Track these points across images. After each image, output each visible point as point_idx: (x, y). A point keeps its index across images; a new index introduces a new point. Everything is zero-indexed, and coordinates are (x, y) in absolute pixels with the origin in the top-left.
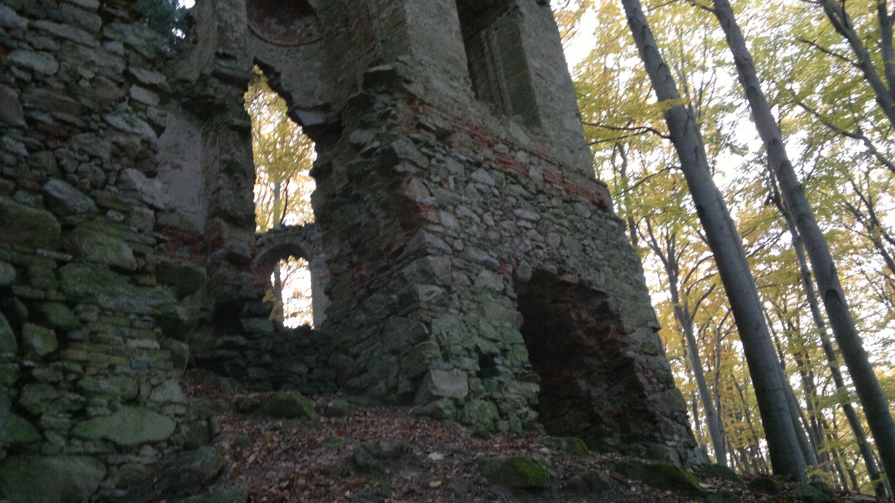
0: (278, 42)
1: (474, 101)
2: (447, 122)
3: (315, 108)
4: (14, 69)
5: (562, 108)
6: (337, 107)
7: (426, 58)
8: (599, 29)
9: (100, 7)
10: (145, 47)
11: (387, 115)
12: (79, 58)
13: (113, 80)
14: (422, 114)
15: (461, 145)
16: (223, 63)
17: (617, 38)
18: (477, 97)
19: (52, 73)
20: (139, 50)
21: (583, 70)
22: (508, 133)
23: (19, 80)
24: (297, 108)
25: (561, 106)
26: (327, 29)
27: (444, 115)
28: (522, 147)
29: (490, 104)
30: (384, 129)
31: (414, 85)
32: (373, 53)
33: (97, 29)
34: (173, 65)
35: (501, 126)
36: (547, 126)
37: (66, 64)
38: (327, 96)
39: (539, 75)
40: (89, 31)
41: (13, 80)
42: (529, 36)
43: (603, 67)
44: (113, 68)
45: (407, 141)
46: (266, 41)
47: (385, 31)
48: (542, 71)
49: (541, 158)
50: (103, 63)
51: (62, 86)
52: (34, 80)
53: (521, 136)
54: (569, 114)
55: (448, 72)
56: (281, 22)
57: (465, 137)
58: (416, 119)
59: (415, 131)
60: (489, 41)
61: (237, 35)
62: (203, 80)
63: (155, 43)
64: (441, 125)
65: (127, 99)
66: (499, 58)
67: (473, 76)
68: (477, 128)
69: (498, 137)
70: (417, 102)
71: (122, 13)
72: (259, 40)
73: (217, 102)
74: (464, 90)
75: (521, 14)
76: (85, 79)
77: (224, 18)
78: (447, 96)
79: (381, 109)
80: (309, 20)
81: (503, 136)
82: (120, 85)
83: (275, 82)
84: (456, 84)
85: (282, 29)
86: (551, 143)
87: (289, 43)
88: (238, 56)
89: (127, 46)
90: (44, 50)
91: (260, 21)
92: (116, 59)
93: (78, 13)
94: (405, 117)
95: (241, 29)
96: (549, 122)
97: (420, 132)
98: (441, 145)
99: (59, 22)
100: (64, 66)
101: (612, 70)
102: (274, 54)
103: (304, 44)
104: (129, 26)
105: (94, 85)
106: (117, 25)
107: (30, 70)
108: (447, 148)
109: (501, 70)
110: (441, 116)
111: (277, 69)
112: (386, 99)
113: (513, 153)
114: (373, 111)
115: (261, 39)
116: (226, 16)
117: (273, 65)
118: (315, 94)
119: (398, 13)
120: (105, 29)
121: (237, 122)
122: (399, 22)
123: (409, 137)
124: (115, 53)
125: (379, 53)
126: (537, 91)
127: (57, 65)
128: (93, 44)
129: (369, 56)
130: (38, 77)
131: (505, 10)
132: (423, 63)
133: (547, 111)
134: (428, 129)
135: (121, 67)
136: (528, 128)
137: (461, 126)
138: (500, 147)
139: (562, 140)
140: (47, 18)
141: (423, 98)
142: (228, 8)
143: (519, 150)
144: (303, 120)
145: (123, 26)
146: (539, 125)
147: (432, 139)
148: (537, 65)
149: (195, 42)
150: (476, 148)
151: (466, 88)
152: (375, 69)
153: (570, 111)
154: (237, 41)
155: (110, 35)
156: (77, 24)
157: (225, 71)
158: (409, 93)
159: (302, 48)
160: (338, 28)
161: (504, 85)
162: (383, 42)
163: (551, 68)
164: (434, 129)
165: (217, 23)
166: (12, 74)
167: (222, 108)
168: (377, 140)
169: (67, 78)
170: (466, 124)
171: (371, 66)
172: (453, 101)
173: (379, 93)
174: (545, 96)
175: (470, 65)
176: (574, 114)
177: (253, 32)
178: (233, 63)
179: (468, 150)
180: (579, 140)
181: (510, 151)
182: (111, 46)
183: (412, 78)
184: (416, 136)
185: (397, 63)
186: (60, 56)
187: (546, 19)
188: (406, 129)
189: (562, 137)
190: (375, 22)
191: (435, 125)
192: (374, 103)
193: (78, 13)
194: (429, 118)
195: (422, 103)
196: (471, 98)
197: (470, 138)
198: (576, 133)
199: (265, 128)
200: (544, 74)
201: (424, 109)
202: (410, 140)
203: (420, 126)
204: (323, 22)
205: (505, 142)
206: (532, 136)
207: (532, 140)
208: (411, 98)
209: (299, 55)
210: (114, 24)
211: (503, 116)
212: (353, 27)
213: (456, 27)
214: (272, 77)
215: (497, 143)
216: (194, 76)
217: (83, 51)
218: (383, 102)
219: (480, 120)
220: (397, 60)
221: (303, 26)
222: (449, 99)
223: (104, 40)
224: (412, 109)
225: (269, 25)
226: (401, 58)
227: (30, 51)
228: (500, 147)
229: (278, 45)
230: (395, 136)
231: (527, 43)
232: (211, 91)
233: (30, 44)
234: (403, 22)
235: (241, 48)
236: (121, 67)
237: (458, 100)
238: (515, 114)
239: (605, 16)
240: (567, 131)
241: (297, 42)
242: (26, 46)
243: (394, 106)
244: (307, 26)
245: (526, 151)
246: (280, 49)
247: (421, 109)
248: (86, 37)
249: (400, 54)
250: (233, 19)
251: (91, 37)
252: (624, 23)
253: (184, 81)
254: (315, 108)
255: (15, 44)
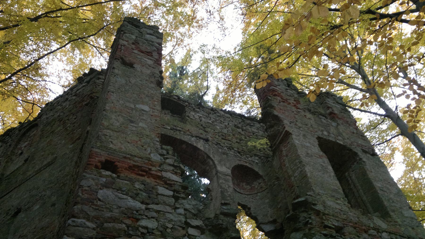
0: (247, 193)
1: (351, 209)
2: (339, 222)
3: (270, 222)
4: (140, 228)
5: (400, 205)
6: (279, 221)
7: (321, 191)
8: (405, 160)
9: (174, 194)
10: (193, 208)
11: (307, 223)
12: (166, 219)
13: (181, 227)
14: (325, 220)
15: (350, 233)
16: (224, 207)
17: (417, 163)
18: (351, 207)
19: (155, 228)
20: (190, 210)
21: (403, 181)
22: (374, 223)
23: (142, 233)
24: (261, 223)
25: (399, 204)
26: (269, 184)
27: (337, 219)
28: (384, 230)
29: (360, 209)
30: (307, 231)
31: (318, 205)
32: (294, 193)
33: (173, 204)
34: (203, 211)
35: (370, 220)
36: (394, 216)
37: (161, 222)
38: (274, 216)
39: (383, 191)
40: (170, 206)
41: (140, 234)
42: (371, 172)
43: (413, 178)
44: (180, 221)
45: (321, 236)
46: (242, 194)
47: (298, 182)
48: (383, 188)
49: (397, 235)
50: (176, 219)
51: (159, 233)
52: (148, 232)
53: (383, 225)
54: (405, 208)
55: (334, 196)
56: (248, 184)
57: (351, 229)
58: (323, 223)
59: (324, 229)
60: (350, 177)
61: (229, 193)
62: (216, 216)
63: (197, 206)
64: (336, 224)
65: (187, 234)
66: (358, 185)
67: (346, 196)
68: (356, 223)
69: (369, 227)
70: (321, 214)
71: (182, 195)
72: (239, 194)
73: (224, 226)
74: (344, 204)
75: (364, 162)
76: (169, 228)
77: (223, 187)
78: (336, 208)
79: (304, 220)
80: (260, 181)
81: (372, 225)
82: (183, 228)
83: (249, 212)
84: (339, 202)
85: (249, 187)
86: (400, 225)
87: (253, 193)
88: (231, 203)
89: (185, 210)
90: (152, 218)
91: (238, 185)
92: (181, 216)
93: (165, 199)
94: (317, 223)
95: (231, 190)
96: (395, 214)
97: (326, 230)
98: (339, 235)
99: (157, 204)
100: (160, 224)
101: (419, 179)
102: (246, 199)
103: (260, 192)
104: (186, 200)
105: (173, 230)
106: (181, 201)
107: (146, 228)
108: (343, 237)
109: (361, 190)
110: (335, 220)
111: (249, 206)
112: (305, 215)
113: (379, 234)
114: (300, 222)
115: (240, 193)
116: (223, 186)
117: (247, 204)
118: (268, 215)
119: (302, 173)
120: (176, 204)
121: (234, 235)
122: (304, 176)
123: (320, 233)
124: (180, 214)
125: (297, 192)
126: (383, 199)
127: (157, 223)
128: (171, 212)
129: (293, 195)
130: (150, 231)
131: (355, 162)
132: (320, 194)
133: (392, 208)
134: (330, 228)
135: (183, 220)
136: (384, 219)
137: (348, 224)
138: (372, 232)
139: (405, 223)
140: (153, 203)
141: (324, 211)
142: (224, 182)
143: (382, 232)
144: (264, 229)
145: (183, 201)
146: (390, 216)
147: (334, 233)
148: (379, 185)
149: (211, 200)
150: (358, 234)
151: (345, 203)
152: (297, 201)
153: (405, 206)
154: (230, 196)
155: (178, 206)
156: (165, 203)
157: (226, 211)
158: (316, 210)
159: (259, 194)
160: (274, 182)
161: (365, 198)
162: (298, 187)
163: (388, 186)
164: (333, 227)
165: (220, 190)
166: (139, 231)
167: (226, 229)
168: (305, 237)
169: (161, 229)
170: (350, 222)
171: (294, 199)
172: (340, 211)
173: (301, 212)
174: (389, 200)
175: (344, 190)
176: (408, 207)
177: (236, 190)
178: (229, 207)
179: (354, 236)
180: (415, 221)
181: (378, 234)
182: (179, 211)
183: (316, 202)
184: (325, 232)
185: (307, 196)
186: (158, 219)
187: (377, 162)
188: (319, 229)
189: (405, 221)
190: (293, 178)
191: (334, 225)
192: (299, 218)
193: (165, 199)
194: (329, 222)
195: (324, 214)
196: (349, 208)
197: (353, 229)
198: (412, 218)
199: (245, 234)
200: (385, 189)
201: (326, 217)
202: (322, 235)
203: (326, 227)
204: (266, 181)
205: (374, 229)
206: (387, 223)
207: (388, 225)
208: (318, 213)
209: (258, 198)
210: (179, 201)
211: (369, 215)
212: (282, 181)
213: (333, 174)
214: (247, 210)
215: (369, 230)
216: (212, 216)
217: (168, 215)
218: (304, 217)
219: (357, 219)
220: (307, 195)
221: (258, 184)
222: (337, 210)
223: (176, 208)
224: (320, 218)
225: (243, 186)
226: (308, 193)
227: (146, 219)
228: (372, 232)
229: (247, 195)
230: (313, 234)
231: (371, 175)
232: (221, 222)
233: (146, 216)
234: (306, 176)
235: (231, 199)
236: (183, 220)
237: (342, 209)
238: (375, 212)
239: (406, 153)
240: (407, 217)
241: (256, 192)
242: (145, 217)
243: (310, 218)
244: (259, 184)
245: (386, 232)
246: (249, 196)
247: (324, 217)
248: (169, 209)
249: (308, 192)
250: (227, 186)
251: (170, 209)
252: (419, 155)
253: (208, 219)
254: (270, 222)
255: (140, 217)
